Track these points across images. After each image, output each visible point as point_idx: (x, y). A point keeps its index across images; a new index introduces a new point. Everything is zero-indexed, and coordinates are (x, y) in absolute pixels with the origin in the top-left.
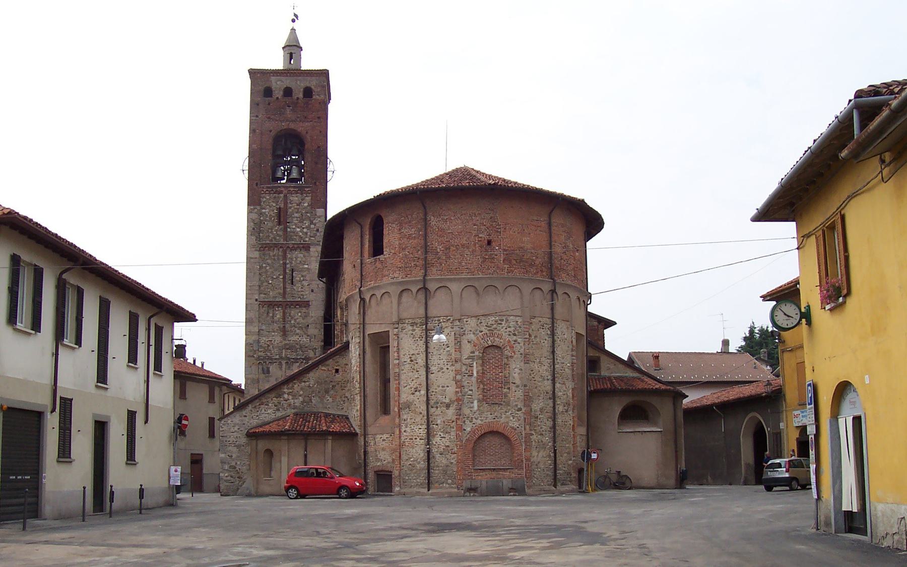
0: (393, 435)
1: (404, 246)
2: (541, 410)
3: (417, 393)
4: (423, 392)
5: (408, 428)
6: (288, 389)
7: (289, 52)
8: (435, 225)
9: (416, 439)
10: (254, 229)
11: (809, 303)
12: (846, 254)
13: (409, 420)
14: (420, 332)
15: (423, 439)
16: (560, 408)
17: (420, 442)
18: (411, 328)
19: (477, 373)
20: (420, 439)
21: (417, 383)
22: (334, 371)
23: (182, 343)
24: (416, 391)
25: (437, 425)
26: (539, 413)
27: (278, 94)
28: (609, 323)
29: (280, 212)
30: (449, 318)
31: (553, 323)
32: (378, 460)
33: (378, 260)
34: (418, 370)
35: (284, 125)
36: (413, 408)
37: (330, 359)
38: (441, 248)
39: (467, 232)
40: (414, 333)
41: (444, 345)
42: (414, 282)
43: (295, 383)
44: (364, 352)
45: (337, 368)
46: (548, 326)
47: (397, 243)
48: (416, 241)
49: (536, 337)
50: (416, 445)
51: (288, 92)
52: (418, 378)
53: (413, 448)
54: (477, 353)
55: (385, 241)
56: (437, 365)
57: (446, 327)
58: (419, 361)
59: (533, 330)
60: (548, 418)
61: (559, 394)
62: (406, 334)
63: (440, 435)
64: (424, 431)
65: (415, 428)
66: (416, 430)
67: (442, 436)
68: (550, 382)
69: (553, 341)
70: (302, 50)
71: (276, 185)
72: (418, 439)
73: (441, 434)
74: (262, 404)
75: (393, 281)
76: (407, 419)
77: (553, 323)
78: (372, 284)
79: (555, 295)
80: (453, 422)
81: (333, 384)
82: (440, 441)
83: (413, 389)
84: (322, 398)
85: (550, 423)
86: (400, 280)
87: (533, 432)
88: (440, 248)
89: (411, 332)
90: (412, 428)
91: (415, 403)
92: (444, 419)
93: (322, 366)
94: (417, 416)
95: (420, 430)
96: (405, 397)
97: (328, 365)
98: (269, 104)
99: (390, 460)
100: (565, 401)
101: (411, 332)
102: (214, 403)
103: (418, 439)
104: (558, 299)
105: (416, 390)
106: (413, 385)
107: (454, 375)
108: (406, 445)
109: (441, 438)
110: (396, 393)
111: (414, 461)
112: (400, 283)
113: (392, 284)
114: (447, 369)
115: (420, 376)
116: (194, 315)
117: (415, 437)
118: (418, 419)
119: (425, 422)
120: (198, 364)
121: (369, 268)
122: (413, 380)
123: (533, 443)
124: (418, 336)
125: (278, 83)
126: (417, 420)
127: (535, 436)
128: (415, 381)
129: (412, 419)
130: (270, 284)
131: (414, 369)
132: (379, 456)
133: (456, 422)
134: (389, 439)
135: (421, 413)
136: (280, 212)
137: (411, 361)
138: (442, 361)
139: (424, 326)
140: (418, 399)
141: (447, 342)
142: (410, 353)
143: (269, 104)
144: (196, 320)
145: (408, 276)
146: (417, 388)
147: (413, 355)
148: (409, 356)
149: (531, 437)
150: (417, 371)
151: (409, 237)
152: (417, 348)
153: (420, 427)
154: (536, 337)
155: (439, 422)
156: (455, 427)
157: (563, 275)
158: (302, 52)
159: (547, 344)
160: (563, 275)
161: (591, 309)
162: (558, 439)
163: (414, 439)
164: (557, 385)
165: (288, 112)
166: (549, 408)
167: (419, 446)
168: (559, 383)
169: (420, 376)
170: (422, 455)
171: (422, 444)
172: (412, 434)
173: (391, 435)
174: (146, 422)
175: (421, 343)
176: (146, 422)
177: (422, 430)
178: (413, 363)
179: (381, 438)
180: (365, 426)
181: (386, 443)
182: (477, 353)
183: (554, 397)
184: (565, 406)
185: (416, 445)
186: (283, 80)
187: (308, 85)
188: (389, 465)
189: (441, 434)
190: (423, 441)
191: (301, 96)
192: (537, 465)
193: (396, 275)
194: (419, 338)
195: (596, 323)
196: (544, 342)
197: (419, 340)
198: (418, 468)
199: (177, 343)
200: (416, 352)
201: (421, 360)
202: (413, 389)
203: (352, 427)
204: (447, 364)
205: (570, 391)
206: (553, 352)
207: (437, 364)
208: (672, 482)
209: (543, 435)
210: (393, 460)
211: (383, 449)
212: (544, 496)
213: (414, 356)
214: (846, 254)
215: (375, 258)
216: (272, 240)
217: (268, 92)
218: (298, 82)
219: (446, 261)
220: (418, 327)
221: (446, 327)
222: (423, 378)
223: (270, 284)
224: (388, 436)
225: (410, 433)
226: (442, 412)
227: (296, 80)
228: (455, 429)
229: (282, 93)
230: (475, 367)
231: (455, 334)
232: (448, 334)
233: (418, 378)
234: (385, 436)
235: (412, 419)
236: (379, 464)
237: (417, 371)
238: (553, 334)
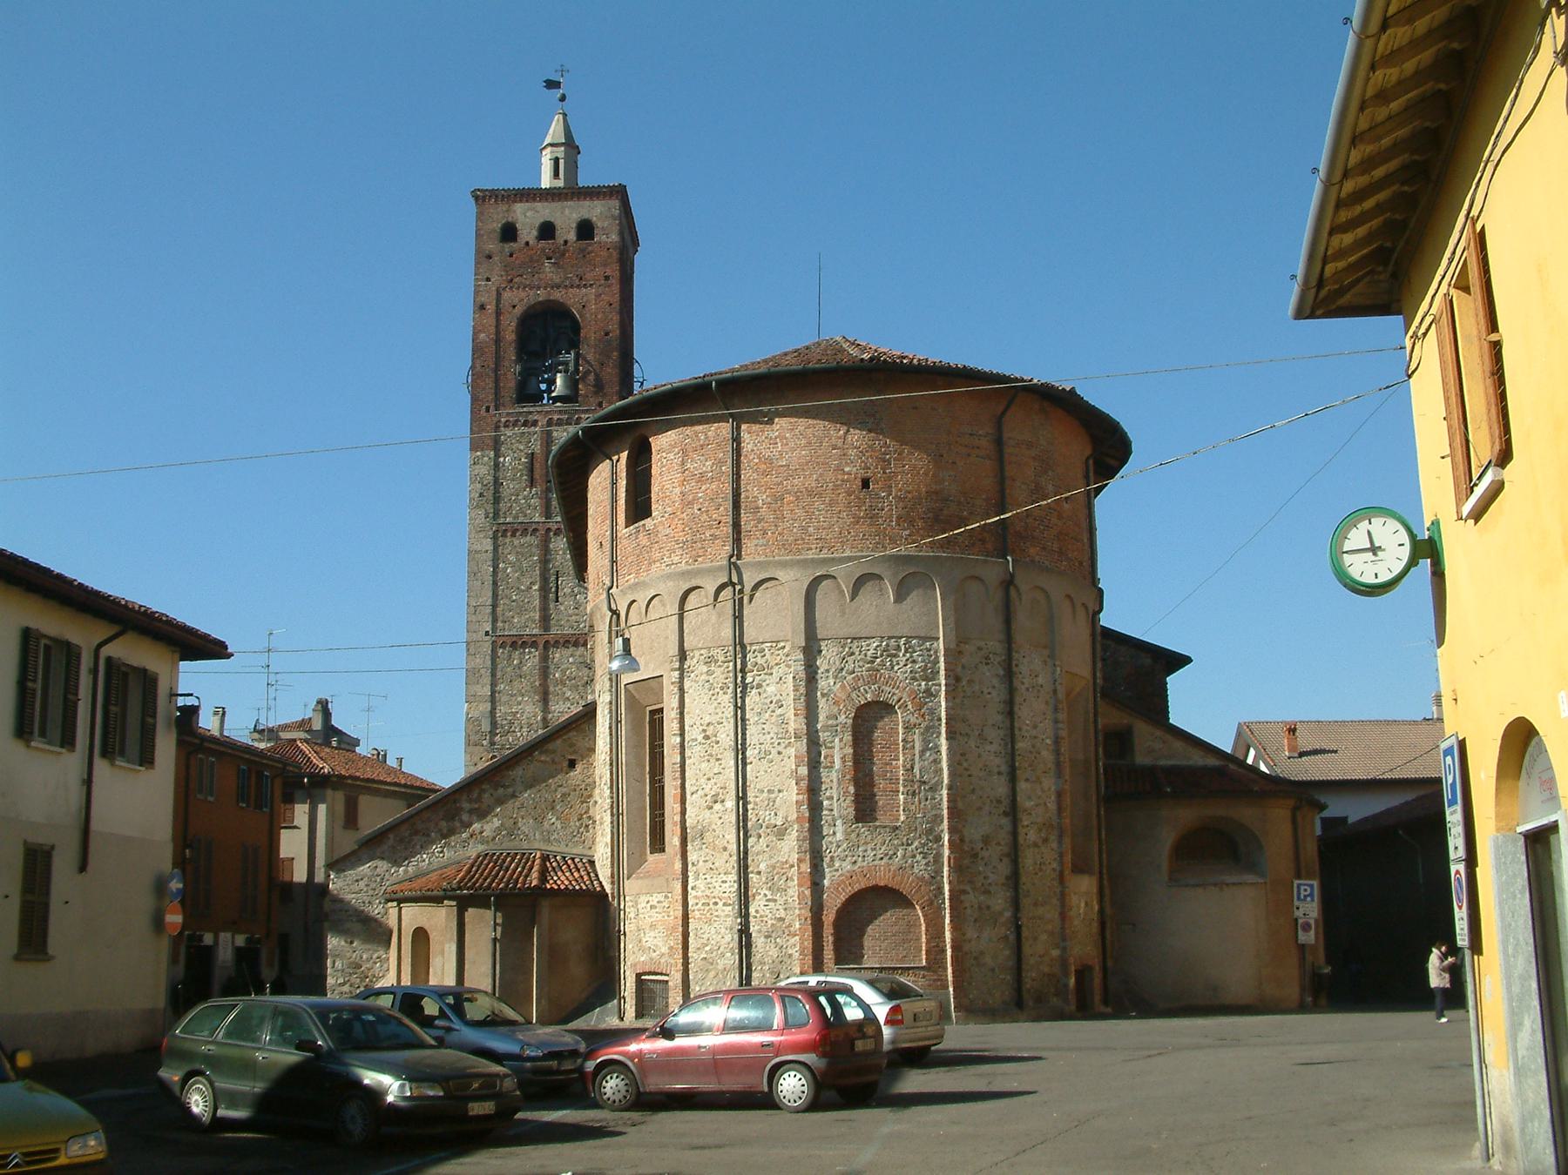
0: (670, 895)
1: (691, 497)
2: (986, 840)
3: (717, 807)
4: (730, 804)
5: (700, 881)
6: (470, 801)
7: (554, 157)
8: (753, 450)
9: (716, 904)
10: (481, 495)
11: (1438, 517)
12: (1494, 337)
13: (701, 863)
14: (725, 676)
15: (730, 905)
16: (1029, 835)
17: (723, 911)
18: (705, 669)
19: (843, 759)
20: (725, 904)
21: (718, 785)
22: (566, 764)
23: (190, 701)
24: (716, 802)
25: (759, 873)
26: (981, 845)
27: (527, 233)
28: (1177, 661)
29: (532, 460)
30: (782, 644)
31: (1009, 650)
32: (642, 950)
33: (641, 528)
34: (719, 756)
35: (542, 295)
36: (708, 837)
37: (558, 738)
38: (765, 497)
39: (818, 463)
40: (711, 678)
41: (771, 702)
42: (710, 571)
43: (484, 791)
44: (618, 722)
45: (573, 757)
46: (998, 659)
47: (678, 490)
48: (713, 487)
49: (970, 682)
50: (717, 916)
51: (547, 231)
52: (720, 773)
53: (709, 922)
54: (842, 718)
55: (655, 489)
56: (758, 746)
57: (777, 664)
58: (722, 737)
59: (963, 667)
60: (1002, 855)
61: (1025, 802)
62: (697, 682)
63: (766, 895)
64: (733, 886)
65: (713, 880)
66: (717, 885)
67: (769, 897)
68: (1004, 779)
69: (1011, 691)
70: (579, 153)
71: (539, 409)
72: (721, 904)
73: (767, 892)
74: (416, 833)
75: (669, 571)
76: (698, 861)
77: (1009, 650)
78: (632, 579)
79: (1013, 592)
80: (792, 866)
81: (564, 790)
82: (765, 908)
83: (709, 798)
84: (539, 820)
85: (1004, 868)
86: (683, 567)
87: (968, 888)
88: (763, 499)
89: (704, 677)
90: (709, 880)
91: (714, 826)
92: (774, 861)
93: (541, 753)
94: (718, 855)
95: (724, 885)
96: (693, 815)
97: (554, 752)
98: (511, 255)
99: (665, 950)
100: (1040, 820)
101: (704, 677)
102: (358, 829)
103: (721, 904)
104: (1020, 599)
105: (715, 798)
106: (710, 788)
107: (794, 767)
108: (696, 917)
109: (767, 900)
110: (675, 806)
111: (711, 951)
112: (684, 574)
113: (669, 576)
114: (779, 753)
115: (724, 769)
116: (223, 645)
117: (714, 900)
118: (720, 861)
119: (733, 867)
120: (391, 762)
121: (625, 546)
122: (709, 779)
123: (969, 911)
124: (720, 685)
125: (528, 214)
126: (717, 864)
127: (971, 896)
128: (712, 781)
129: (707, 861)
130: (513, 601)
131: (711, 755)
132: (644, 940)
133: (799, 867)
134: (664, 904)
135: (725, 849)
136: (532, 460)
137: (706, 737)
138: (768, 737)
139: (731, 664)
140: (720, 818)
141: (778, 697)
142: (702, 722)
143: (511, 255)
144: (229, 656)
145: (699, 559)
146: (717, 795)
147: (708, 725)
148: (701, 728)
149: (962, 898)
150: (718, 760)
151: (702, 478)
152: (717, 711)
153: (724, 879)
154: (970, 682)
155: (762, 867)
156: (796, 878)
157: (1032, 551)
158: (579, 156)
159: (996, 695)
160: (1032, 551)
161: (1106, 620)
162: (1025, 902)
163: (711, 906)
164: (1022, 786)
165: (548, 269)
166: (1004, 836)
167: (722, 919)
168: (1027, 780)
169: (724, 769)
170: (728, 938)
171: (727, 916)
172: (708, 892)
173: (666, 897)
174: (83, 867)
175: (726, 699)
176: (83, 867)
177: (727, 885)
178: (708, 742)
179: (648, 902)
180: (616, 879)
181: (657, 913)
182: (842, 718)
183: (1013, 811)
184: (1040, 830)
185: (717, 916)
186: (538, 209)
187: (586, 216)
188: (663, 961)
189: (767, 892)
190: (730, 908)
191: (572, 236)
192: (976, 958)
193: (676, 559)
194: (722, 688)
195: (1148, 661)
196: (989, 693)
197: (721, 692)
198: (720, 967)
199: (181, 702)
200: (717, 718)
201: (726, 735)
202: (709, 798)
203: (598, 879)
204: (779, 744)
205: (1053, 798)
206: (1010, 714)
207: (757, 743)
208: (1293, 992)
209: (989, 892)
210: (671, 948)
211: (653, 926)
212: (83, 1156)
213: (711, 727)
214: (1494, 337)
215: (636, 525)
216: (516, 517)
217: (509, 232)
218: (567, 211)
219: (776, 526)
220: (720, 666)
221: (777, 664)
222: (730, 773)
223: (513, 601)
224: (661, 897)
225: (703, 891)
226: (767, 846)
227: (563, 208)
228: (796, 882)
229: (535, 233)
230: (837, 748)
231: (794, 677)
232: (781, 679)
233: (720, 773)
234: (655, 899)
235: (707, 861)
236: (642, 959)
237: (718, 760)
238: (1009, 674)
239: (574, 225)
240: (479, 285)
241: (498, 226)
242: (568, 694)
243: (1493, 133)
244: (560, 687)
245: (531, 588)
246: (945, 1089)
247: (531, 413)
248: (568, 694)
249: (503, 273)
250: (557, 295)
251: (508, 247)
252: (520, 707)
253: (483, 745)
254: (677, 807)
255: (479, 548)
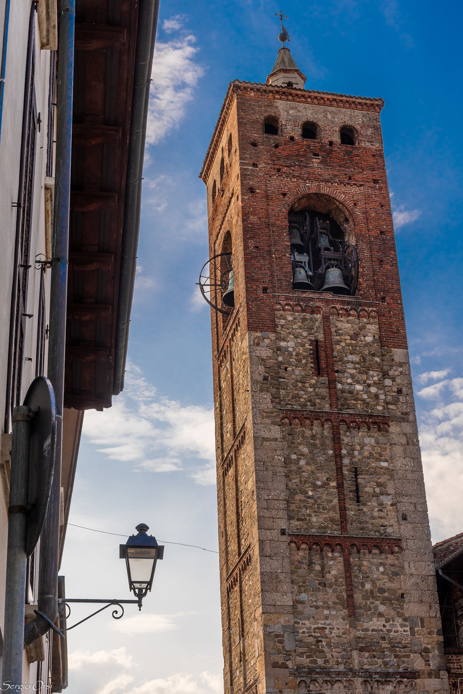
98: (276, 146)
191: (336, 139)
239: (337, 129)
240: (246, 169)
241: (261, 118)
242: (382, 608)
243: (59, 657)
244: (372, 600)
245: (328, 484)
246: (18, 191)
247: (312, 299)
248: (382, 608)
249: (270, 162)
250: (325, 190)
251: (273, 139)
252: (328, 622)
253: (287, 667)
254: (230, 416)
255: (267, 435)
